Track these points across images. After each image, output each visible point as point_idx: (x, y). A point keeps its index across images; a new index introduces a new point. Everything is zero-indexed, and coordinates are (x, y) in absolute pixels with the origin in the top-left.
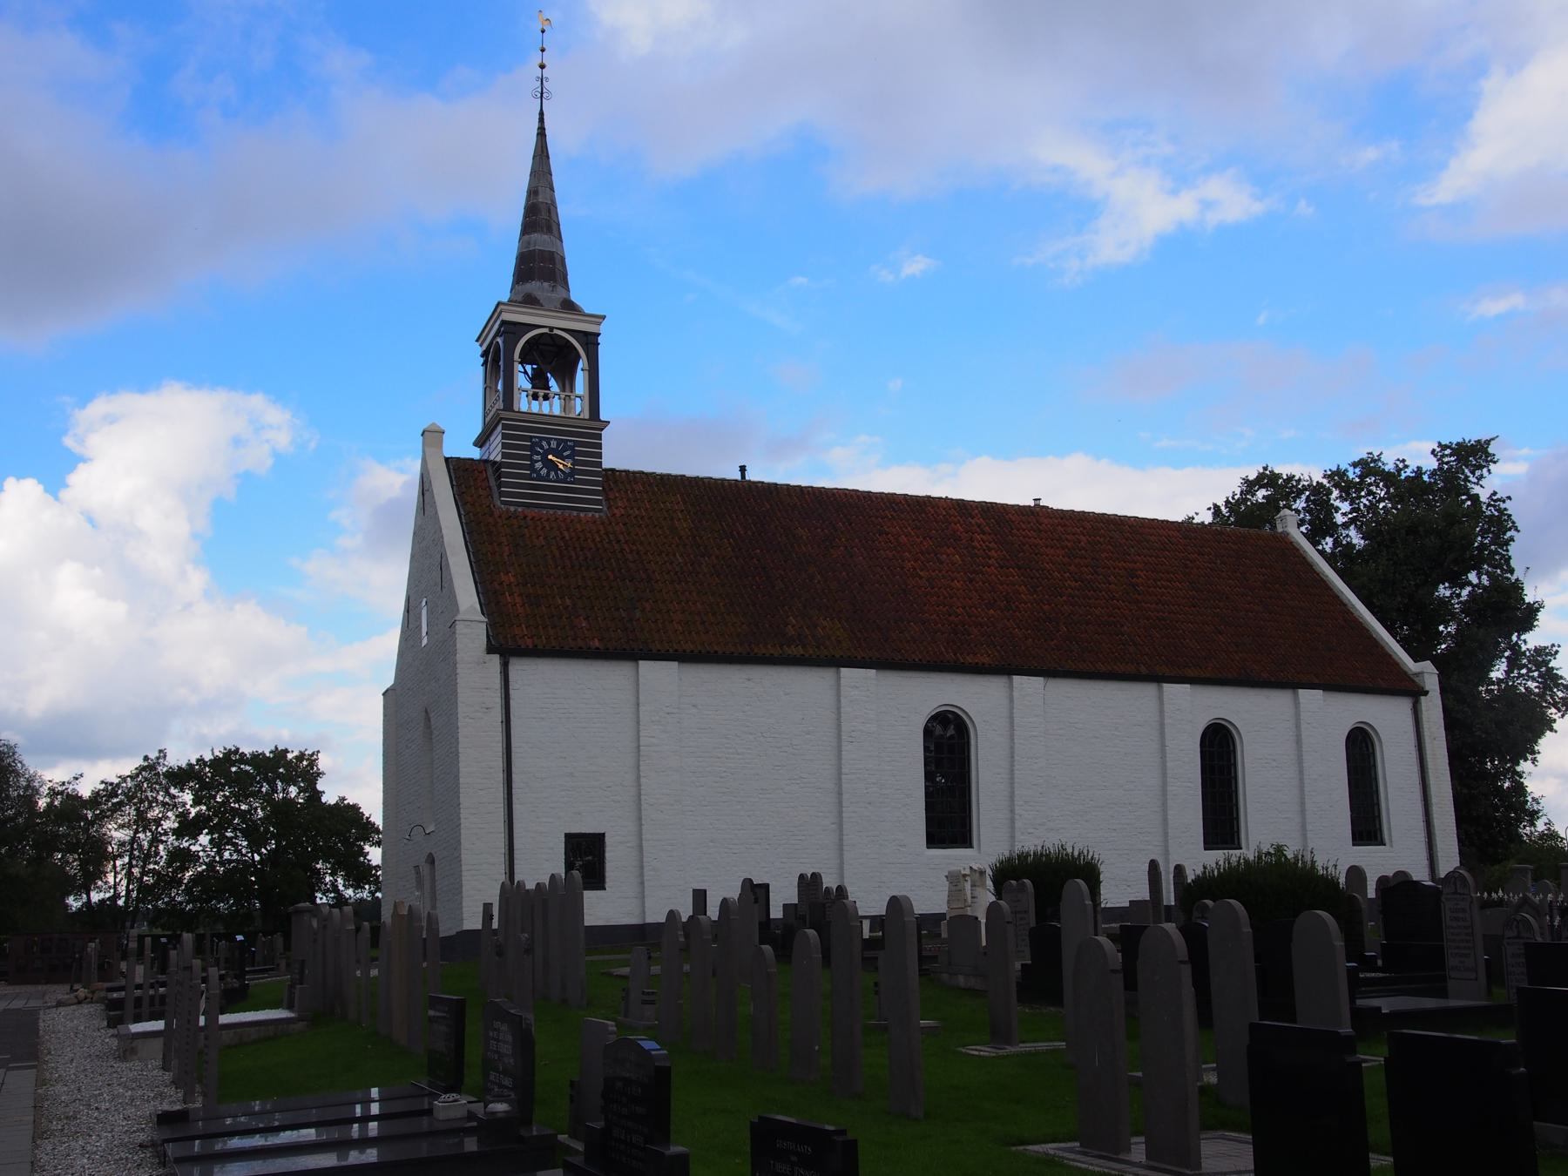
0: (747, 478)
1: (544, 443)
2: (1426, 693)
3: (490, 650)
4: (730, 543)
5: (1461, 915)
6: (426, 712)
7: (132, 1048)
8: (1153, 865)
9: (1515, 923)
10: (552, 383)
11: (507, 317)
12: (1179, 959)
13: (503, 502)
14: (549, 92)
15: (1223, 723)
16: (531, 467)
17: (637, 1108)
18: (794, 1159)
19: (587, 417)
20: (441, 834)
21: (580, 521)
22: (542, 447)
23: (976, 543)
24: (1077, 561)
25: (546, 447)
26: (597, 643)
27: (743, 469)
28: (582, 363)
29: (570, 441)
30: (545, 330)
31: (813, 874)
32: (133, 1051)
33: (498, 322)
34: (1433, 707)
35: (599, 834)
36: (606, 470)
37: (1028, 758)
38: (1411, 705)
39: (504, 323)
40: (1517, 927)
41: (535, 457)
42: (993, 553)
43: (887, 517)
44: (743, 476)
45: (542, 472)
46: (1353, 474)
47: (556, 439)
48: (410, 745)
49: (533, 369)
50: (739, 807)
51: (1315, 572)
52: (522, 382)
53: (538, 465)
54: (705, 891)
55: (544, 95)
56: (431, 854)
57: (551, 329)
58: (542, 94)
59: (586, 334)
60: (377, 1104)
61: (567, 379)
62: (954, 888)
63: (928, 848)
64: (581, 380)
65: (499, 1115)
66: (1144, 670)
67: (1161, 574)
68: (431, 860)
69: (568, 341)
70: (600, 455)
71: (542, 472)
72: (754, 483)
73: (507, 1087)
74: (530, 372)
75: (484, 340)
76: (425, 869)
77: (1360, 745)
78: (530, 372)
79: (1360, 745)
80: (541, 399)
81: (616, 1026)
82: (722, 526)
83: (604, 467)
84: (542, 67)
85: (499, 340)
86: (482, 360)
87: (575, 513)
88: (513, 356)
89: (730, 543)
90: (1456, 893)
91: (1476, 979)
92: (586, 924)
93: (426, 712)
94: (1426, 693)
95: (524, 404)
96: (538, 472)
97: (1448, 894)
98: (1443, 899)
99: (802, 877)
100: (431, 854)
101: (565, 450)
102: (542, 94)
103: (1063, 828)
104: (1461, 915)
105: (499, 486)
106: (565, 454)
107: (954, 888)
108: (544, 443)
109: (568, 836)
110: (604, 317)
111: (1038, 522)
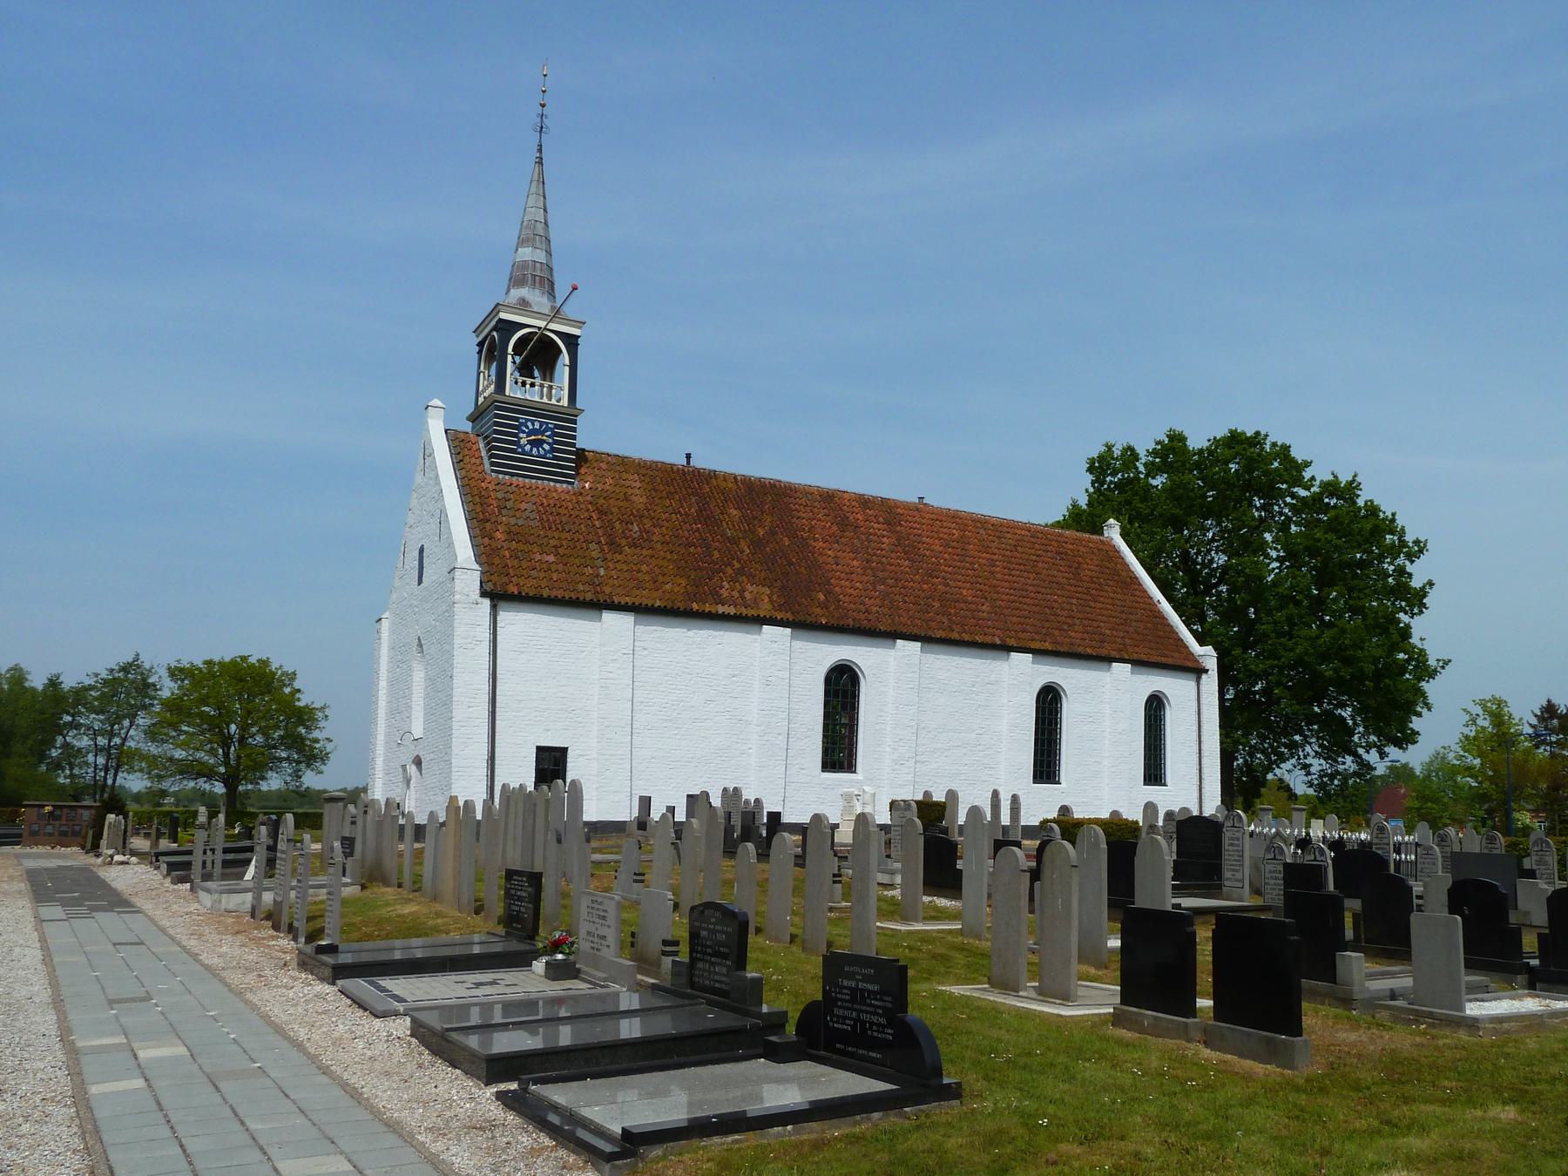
0: (692, 464)
1: (529, 424)
2: (1206, 671)
3: (484, 594)
8: (995, 794)
10: (536, 373)
11: (503, 316)
12: (1021, 868)
13: (493, 471)
14: (547, 127)
16: (517, 443)
19: (566, 405)
20: (429, 740)
21: (556, 491)
22: (527, 427)
25: (531, 427)
27: (688, 456)
28: (565, 357)
31: (736, 789)
33: (496, 319)
34: (1211, 682)
35: (563, 748)
39: (501, 320)
40: (1274, 852)
41: (521, 435)
44: (688, 462)
45: (526, 448)
50: (676, 732)
53: (523, 441)
54: (650, 797)
56: (418, 756)
58: (542, 128)
60: (399, 951)
61: (548, 371)
62: (847, 805)
63: (822, 771)
66: (1012, 642)
69: (556, 342)
70: (574, 438)
71: (526, 448)
72: (698, 470)
75: (481, 332)
77: (1155, 707)
78: (518, 362)
79: (1155, 707)
80: (528, 386)
81: (673, 895)
84: (543, 106)
87: (552, 484)
88: (507, 350)
90: (1233, 826)
92: (584, 820)
94: (1206, 671)
96: (522, 447)
98: (1224, 830)
99: (725, 790)
100: (418, 756)
102: (542, 128)
103: (926, 761)
105: (490, 457)
107: (847, 805)
108: (529, 424)
109: (540, 750)
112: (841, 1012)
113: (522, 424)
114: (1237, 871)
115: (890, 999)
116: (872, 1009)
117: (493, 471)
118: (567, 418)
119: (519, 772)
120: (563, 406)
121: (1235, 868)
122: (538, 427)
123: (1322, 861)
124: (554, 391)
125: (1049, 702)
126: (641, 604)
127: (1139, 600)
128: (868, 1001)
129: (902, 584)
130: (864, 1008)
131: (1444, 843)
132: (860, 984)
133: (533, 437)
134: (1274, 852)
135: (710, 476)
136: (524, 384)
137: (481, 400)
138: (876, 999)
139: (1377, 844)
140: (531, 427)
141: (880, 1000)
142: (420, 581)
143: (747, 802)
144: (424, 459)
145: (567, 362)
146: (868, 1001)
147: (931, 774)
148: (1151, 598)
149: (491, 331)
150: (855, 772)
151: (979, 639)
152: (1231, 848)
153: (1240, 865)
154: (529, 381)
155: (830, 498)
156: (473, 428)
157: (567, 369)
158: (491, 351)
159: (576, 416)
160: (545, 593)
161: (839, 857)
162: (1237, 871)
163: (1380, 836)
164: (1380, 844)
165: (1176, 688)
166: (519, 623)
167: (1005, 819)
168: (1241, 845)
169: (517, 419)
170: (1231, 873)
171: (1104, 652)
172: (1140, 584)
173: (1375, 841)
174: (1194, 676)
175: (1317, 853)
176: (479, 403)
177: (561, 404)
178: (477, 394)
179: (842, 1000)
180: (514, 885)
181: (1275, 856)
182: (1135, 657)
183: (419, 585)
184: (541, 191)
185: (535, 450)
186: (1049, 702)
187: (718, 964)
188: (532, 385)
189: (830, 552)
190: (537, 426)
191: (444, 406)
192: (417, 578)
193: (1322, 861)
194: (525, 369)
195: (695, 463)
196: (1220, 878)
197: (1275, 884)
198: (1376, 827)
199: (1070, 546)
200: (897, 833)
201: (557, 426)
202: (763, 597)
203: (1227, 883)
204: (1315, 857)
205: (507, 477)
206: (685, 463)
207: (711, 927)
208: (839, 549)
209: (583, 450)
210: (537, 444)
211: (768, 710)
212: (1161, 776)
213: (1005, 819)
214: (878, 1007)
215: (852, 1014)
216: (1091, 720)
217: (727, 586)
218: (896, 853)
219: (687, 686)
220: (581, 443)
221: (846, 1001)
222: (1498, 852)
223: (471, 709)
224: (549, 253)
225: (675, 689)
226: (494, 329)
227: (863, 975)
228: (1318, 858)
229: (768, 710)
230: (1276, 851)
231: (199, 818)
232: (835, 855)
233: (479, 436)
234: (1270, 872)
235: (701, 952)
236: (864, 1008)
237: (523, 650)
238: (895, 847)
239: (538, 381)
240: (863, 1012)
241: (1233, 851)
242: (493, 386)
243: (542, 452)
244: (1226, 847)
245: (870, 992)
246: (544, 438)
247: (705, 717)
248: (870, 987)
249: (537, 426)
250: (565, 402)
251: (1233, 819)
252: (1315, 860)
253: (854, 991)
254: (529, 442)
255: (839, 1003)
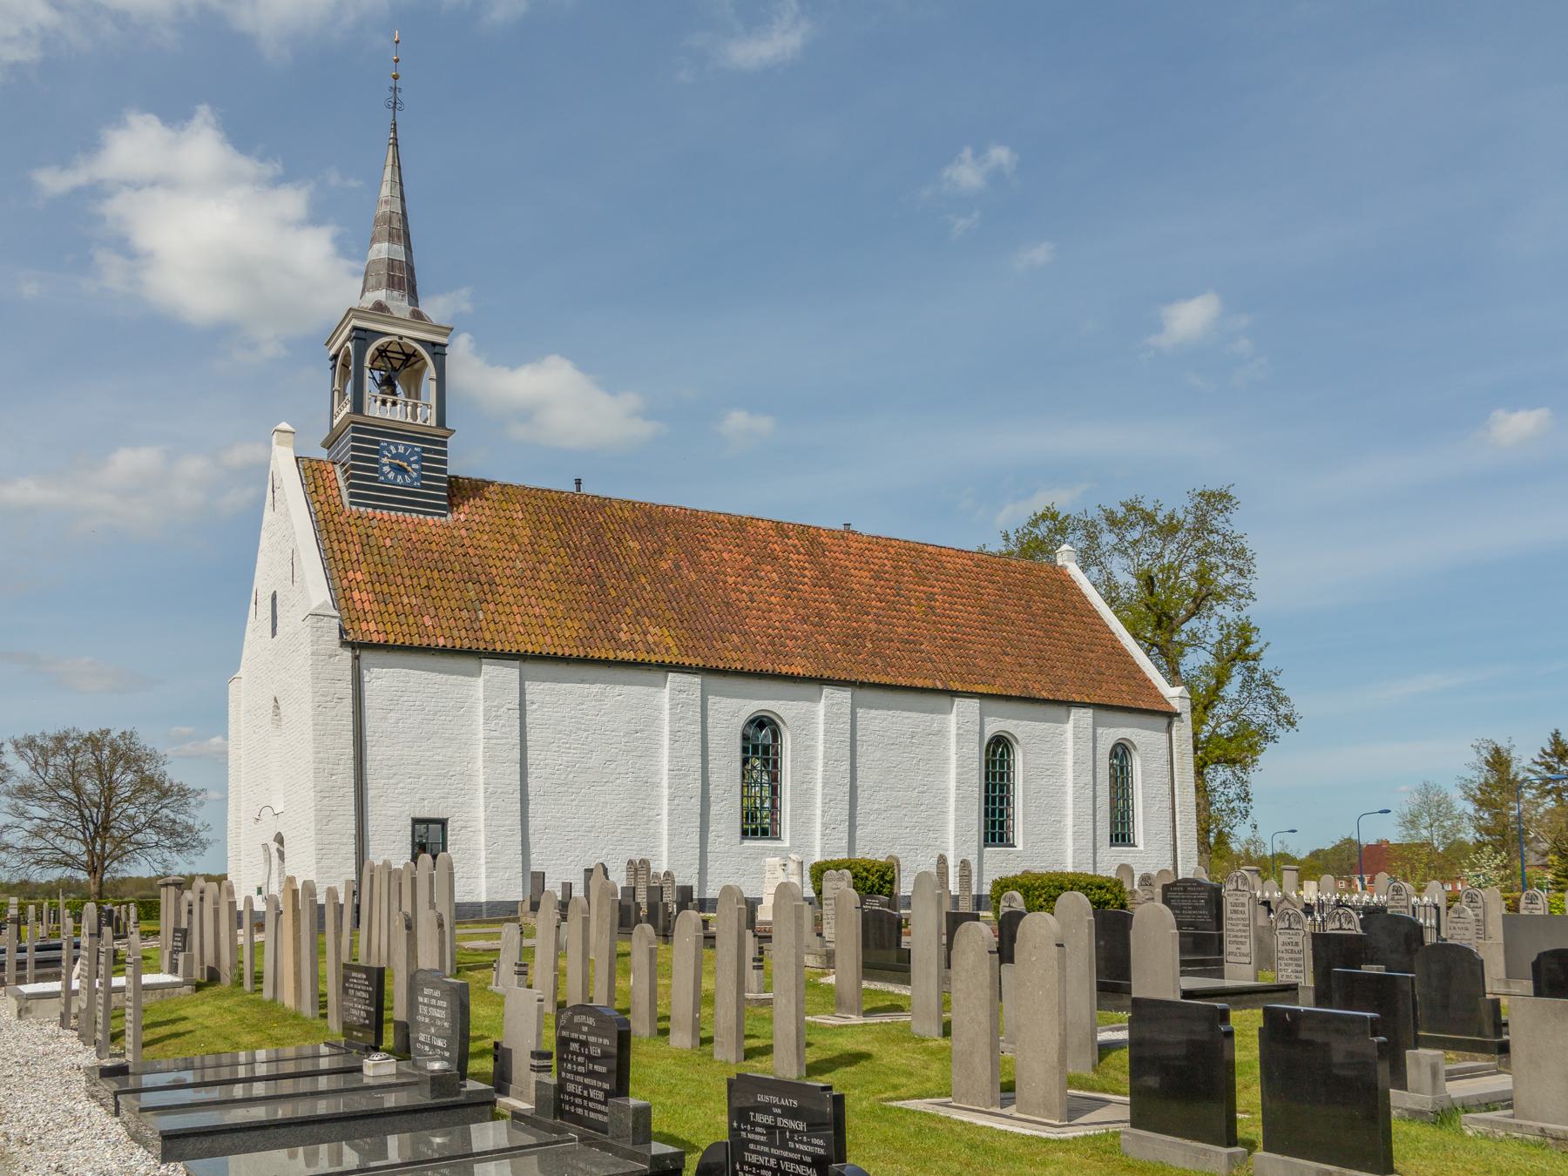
1: (392, 448)
4: (567, 552)
5: (1240, 909)
6: (276, 700)
7: (27, 1008)
9: (1287, 916)
10: (399, 389)
14: (401, 103)
15: (1006, 735)
17: (595, 1067)
18: (777, 1111)
19: (434, 424)
22: (390, 452)
23: (791, 563)
24: (882, 583)
25: (394, 452)
26: (441, 642)
27: (578, 482)
28: (431, 371)
29: (383, 441)
30: (396, 339)
32: (28, 1010)
33: (349, 327)
34: (1183, 731)
36: (450, 477)
37: (835, 761)
38: (1166, 725)
40: (1289, 920)
42: (806, 572)
43: (710, 534)
44: (579, 490)
46: (1120, 512)
47: (403, 445)
48: (257, 730)
49: (381, 375)
51: (1089, 603)
52: (370, 388)
55: (398, 106)
57: (401, 338)
58: (395, 103)
59: (434, 344)
61: (414, 391)
64: (429, 388)
65: (1226, 1053)
66: (956, 686)
67: (955, 599)
68: (280, 839)
70: (444, 462)
73: (440, 1048)
74: (378, 378)
75: (334, 344)
76: (274, 846)
78: (378, 378)
80: (389, 404)
82: (559, 535)
83: (448, 473)
84: (396, 78)
85: (348, 344)
86: (331, 364)
89: (567, 552)
90: (1237, 889)
91: (1250, 963)
92: (456, 901)
93: (276, 700)
95: (374, 410)
96: (385, 475)
97: (1230, 890)
99: (630, 862)
100: (279, 833)
101: (412, 455)
102: (395, 103)
104: (1240, 909)
106: (412, 459)
108: (392, 448)
110: (452, 329)
111: (847, 546)
112: (754, 1159)
113: (383, 448)
114: (1242, 943)
115: (821, 1142)
116: (797, 1156)
117: (352, 503)
118: (433, 442)
119: (391, 848)
120: (431, 427)
121: (1240, 939)
122: (402, 452)
123: (1349, 929)
124: (419, 409)
125: (998, 751)
126: (526, 651)
127: (1099, 635)
128: (791, 1145)
129: (827, 623)
130: (786, 1154)
131: (1475, 905)
132: (779, 1119)
133: (398, 461)
134: (1289, 920)
135: (603, 504)
136: (384, 402)
137: (336, 422)
138: (801, 1142)
139: (1393, 907)
140: (394, 452)
141: (809, 1143)
142: (274, 634)
143: (656, 876)
144: (273, 492)
145: (434, 376)
146: (791, 1145)
147: (868, 839)
148: (1113, 634)
149: (344, 342)
150: (779, 839)
151: (919, 683)
152: (1234, 916)
153: (1245, 937)
154: (390, 398)
155: (740, 526)
156: (329, 455)
157: (433, 385)
158: (346, 367)
159: (446, 437)
160: (416, 641)
161: (760, 937)
162: (1242, 943)
163: (1396, 897)
164: (1397, 907)
165: (1145, 738)
166: (383, 679)
167: (954, 886)
168: (1247, 912)
169: (377, 443)
170: (1235, 946)
171: (1059, 696)
172: (1100, 618)
173: (1391, 903)
174: (1164, 722)
175: (1343, 920)
176: (335, 425)
177: (428, 423)
178: (332, 417)
179: (756, 1142)
180: (354, 983)
181: (1290, 924)
182: (1096, 700)
183: (273, 637)
184: (397, 178)
185: (400, 477)
186: (998, 751)
187: (594, 1088)
188: (394, 403)
189: (744, 588)
190: (401, 449)
191: (293, 430)
192: (270, 630)
193: (1349, 929)
194: (388, 384)
195: (585, 489)
196: (1221, 952)
197: (1291, 959)
198: (1466, 893)
199: (1019, 576)
200: (830, 907)
201: (424, 450)
202: (662, 640)
203: (1230, 958)
204: (1341, 924)
205: (370, 510)
206: (575, 490)
207: (583, 1037)
208: (753, 584)
209: (456, 477)
210: (400, 470)
211: (678, 770)
212: (1129, 836)
213: (954, 886)
214: (807, 1153)
215: (769, 1161)
216: (1049, 773)
217: (625, 629)
218: (829, 930)
219: (583, 744)
220: (454, 468)
221: (761, 1143)
222: (1541, 912)
223: (334, 777)
224: (408, 248)
225: (570, 748)
226: (348, 339)
227: (781, 1107)
228: (1345, 926)
229: (678, 770)
230: (1292, 919)
231: (10, 910)
232: (755, 936)
233: (335, 463)
234: (1284, 944)
235: (571, 1072)
236: (786, 1154)
237: (392, 707)
238: (828, 923)
239: (401, 397)
240: (785, 1159)
241: (1238, 919)
242: (348, 406)
243: (408, 480)
244: (1229, 915)
245: (793, 1131)
246: (409, 469)
247: (604, 780)
248: (793, 1124)
249: (401, 449)
250: (432, 422)
251: (1237, 881)
252: (1341, 929)
253: (770, 1129)
254: (390, 465)
255: (752, 1146)
